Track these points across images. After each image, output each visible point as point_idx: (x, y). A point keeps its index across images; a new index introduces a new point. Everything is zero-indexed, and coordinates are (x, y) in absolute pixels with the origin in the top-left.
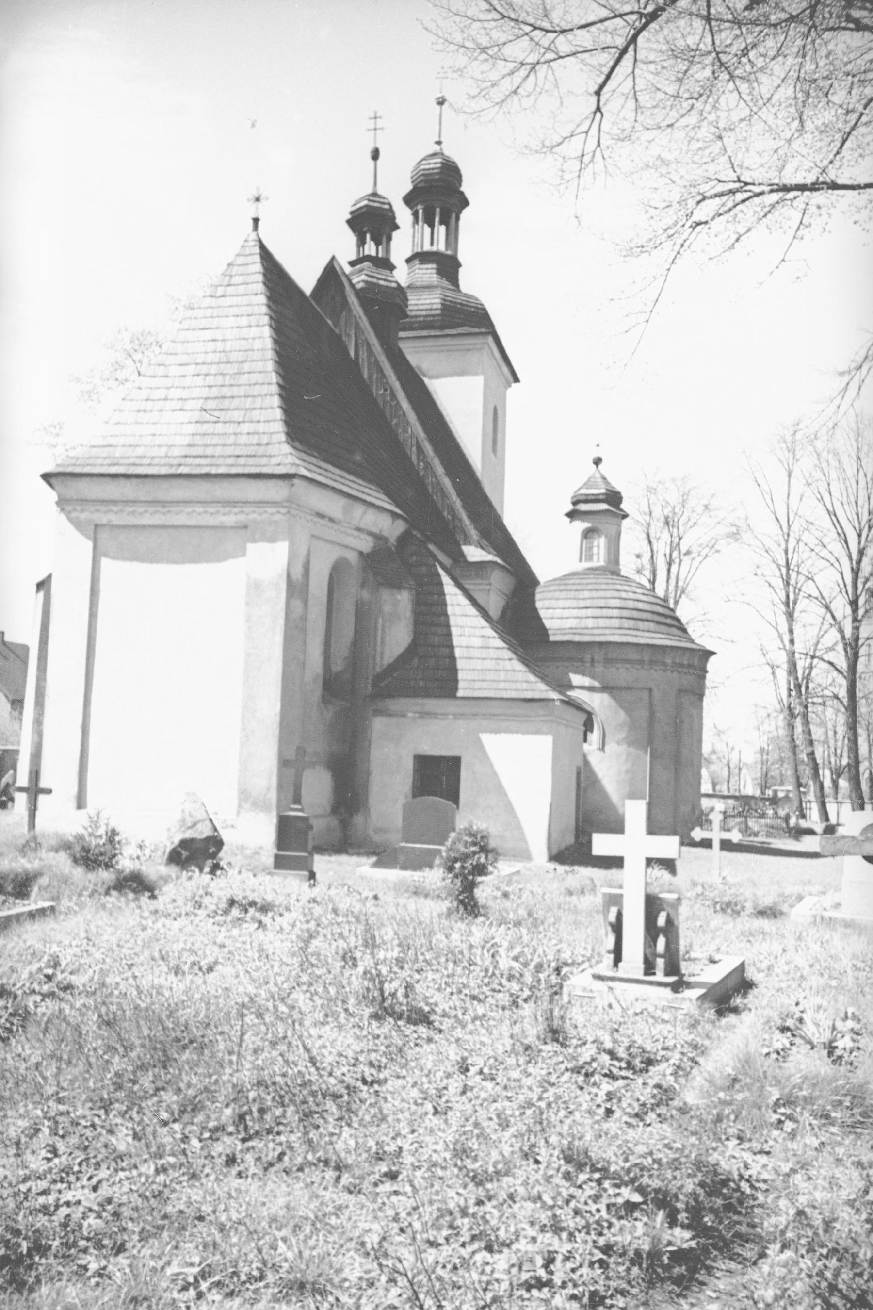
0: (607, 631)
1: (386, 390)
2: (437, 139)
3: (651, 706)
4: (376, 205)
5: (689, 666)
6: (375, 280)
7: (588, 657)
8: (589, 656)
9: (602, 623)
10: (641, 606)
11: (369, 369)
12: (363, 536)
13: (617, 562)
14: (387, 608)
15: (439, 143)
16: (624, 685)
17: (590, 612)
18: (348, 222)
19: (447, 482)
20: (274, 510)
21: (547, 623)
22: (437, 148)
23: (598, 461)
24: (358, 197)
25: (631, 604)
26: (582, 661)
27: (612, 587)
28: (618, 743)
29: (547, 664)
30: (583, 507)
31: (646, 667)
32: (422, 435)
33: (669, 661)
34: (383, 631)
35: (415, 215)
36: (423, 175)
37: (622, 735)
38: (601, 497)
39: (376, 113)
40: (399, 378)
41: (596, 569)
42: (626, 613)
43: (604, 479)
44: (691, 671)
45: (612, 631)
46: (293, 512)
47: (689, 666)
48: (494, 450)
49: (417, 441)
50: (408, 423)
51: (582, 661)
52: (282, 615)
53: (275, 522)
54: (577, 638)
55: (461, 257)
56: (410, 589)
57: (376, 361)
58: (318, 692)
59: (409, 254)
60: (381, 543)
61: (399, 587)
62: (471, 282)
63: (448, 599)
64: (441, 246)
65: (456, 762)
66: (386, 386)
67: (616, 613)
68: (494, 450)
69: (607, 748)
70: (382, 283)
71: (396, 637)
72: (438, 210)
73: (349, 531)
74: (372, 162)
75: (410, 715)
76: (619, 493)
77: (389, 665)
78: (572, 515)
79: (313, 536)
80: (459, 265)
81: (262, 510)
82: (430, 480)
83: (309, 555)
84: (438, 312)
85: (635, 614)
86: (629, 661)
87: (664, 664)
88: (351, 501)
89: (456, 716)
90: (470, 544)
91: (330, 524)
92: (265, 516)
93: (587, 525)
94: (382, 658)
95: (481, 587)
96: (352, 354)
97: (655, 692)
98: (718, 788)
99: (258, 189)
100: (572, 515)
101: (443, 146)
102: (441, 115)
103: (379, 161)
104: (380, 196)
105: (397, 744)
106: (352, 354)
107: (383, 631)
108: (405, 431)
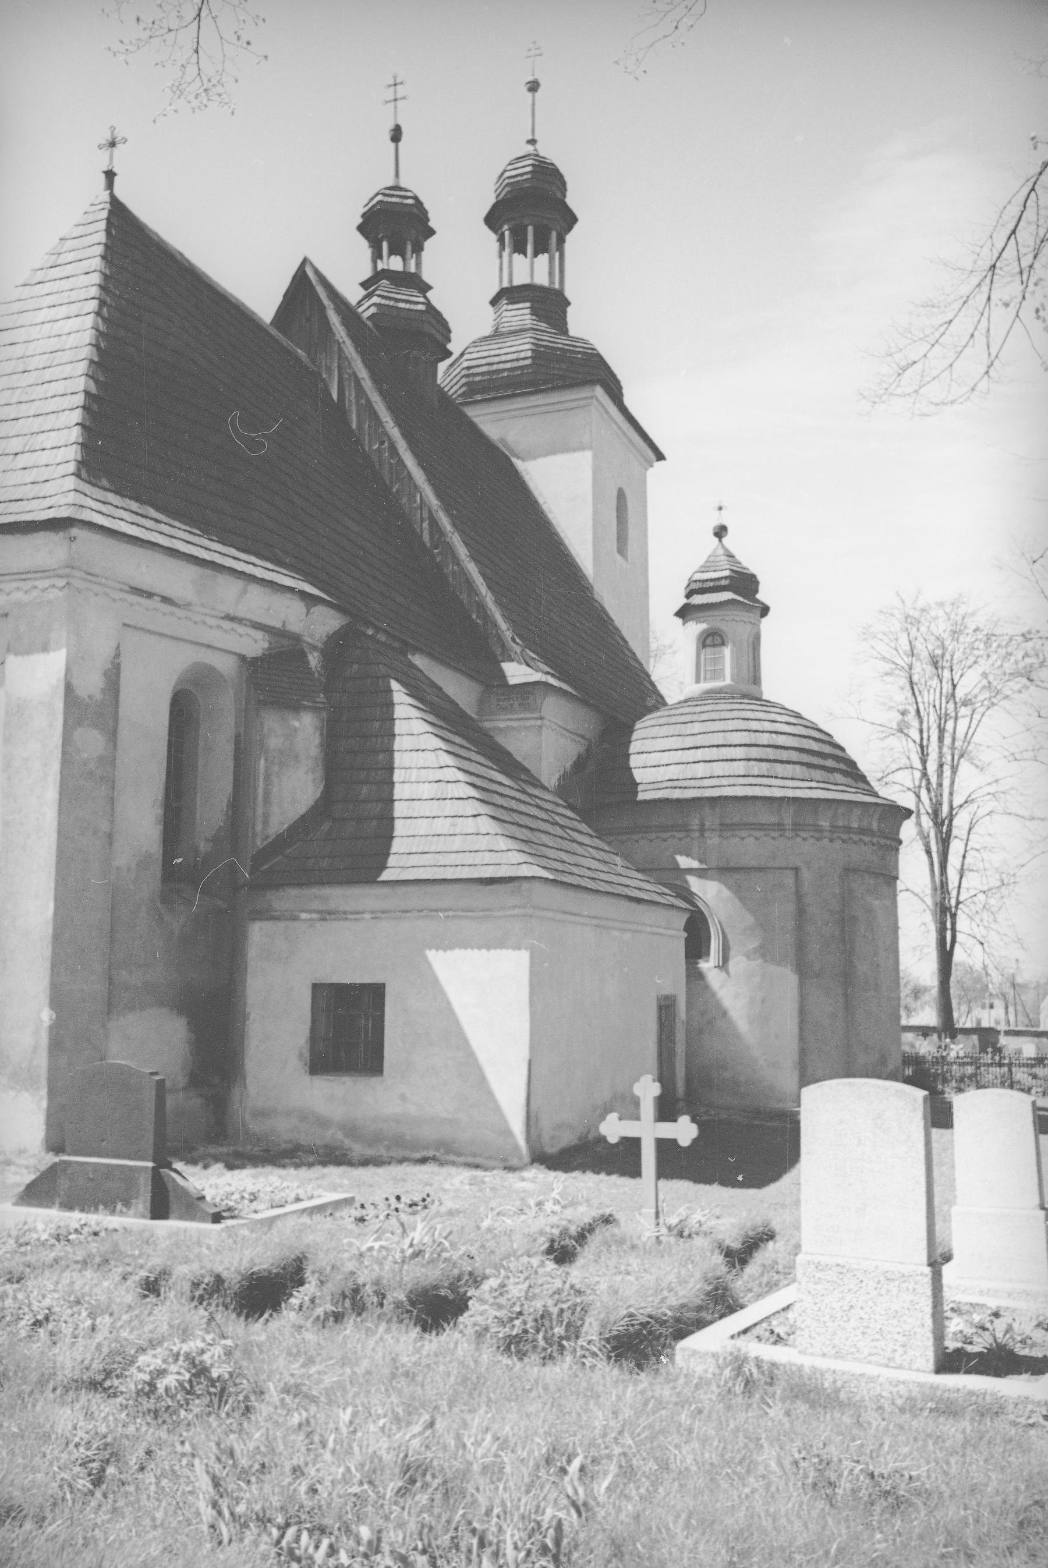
0: (724, 781)
1: (382, 443)
2: (530, 137)
3: (799, 897)
4: (394, 200)
5: (862, 831)
6: (392, 303)
7: (695, 823)
8: (697, 821)
9: (719, 769)
10: (781, 740)
11: (358, 415)
12: (241, 630)
13: (756, 680)
14: (274, 742)
15: (532, 142)
16: (754, 863)
17: (699, 754)
18: (361, 228)
19: (472, 568)
20: (46, 583)
21: (638, 775)
22: (530, 148)
23: (720, 532)
24: (372, 195)
25: (765, 739)
26: (686, 828)
27: (735, 714)
28: (748, 956)
29: (636, 837)
30: (698, 600)
32: (434, 501)
33: (825, 824)
34: (268, 777)
35: (501, 240)
36: (507, 184)
37: (754, 944)
38: (723, 583)
39: (395, 78)
40: (398, 423)
41: (720, 691)
42: (755, 752)
43: (731, 556)
44: (866, 839)
45: (732, 781)
46: (77, 583)
47: (862, 831)
48: (622, 550)
49: (430, 512)
50: (415, 486)
51: (686, 828)
52: (57, 754)
53: (49, 602)
54: (677, 794)
55: (568, 294)
56: (315, 710)
57: (368, 401)
58: (151, 882)
59: (495, 290)
60: (285, 642)
61: (296, 708)
62: (583, 323)
63: (399, 727)
64: (542, 279)
65: (377, 991)
66: (383, 436)
67: (739, 752)
68: (622, 550)
69: (731, 964)
70: (402, 305)
71: (293, 790)
72: (530, 229)
73: (211, 621)
74: (393, 145)
75: (303, 916)
76: (754, 576)
77: (279, 837)
78: (684, 613)
79: (125, 625)
80: (568, 303)
81: (30, 583)
82: (450, 568)
83: (118, 655)
84: (528, 362)
85: (771, 753)
87: (819, 829)
88: (208, 572)
89: (377, 915)
91: (166, 608)
92: (35, 593)
93: (703, 626)
94: (266, 823)
95: (528, 723)
96: (335, 396)
97: (806, 874)
99: (113, 128)
100: (684, 613)
101: (538, 146)
102: (533, 104)
103: (400, 144)
104: (401, 189)
105: (288, 964)
106: (335, 396)
107: (268, 777)
108: (411, 499)
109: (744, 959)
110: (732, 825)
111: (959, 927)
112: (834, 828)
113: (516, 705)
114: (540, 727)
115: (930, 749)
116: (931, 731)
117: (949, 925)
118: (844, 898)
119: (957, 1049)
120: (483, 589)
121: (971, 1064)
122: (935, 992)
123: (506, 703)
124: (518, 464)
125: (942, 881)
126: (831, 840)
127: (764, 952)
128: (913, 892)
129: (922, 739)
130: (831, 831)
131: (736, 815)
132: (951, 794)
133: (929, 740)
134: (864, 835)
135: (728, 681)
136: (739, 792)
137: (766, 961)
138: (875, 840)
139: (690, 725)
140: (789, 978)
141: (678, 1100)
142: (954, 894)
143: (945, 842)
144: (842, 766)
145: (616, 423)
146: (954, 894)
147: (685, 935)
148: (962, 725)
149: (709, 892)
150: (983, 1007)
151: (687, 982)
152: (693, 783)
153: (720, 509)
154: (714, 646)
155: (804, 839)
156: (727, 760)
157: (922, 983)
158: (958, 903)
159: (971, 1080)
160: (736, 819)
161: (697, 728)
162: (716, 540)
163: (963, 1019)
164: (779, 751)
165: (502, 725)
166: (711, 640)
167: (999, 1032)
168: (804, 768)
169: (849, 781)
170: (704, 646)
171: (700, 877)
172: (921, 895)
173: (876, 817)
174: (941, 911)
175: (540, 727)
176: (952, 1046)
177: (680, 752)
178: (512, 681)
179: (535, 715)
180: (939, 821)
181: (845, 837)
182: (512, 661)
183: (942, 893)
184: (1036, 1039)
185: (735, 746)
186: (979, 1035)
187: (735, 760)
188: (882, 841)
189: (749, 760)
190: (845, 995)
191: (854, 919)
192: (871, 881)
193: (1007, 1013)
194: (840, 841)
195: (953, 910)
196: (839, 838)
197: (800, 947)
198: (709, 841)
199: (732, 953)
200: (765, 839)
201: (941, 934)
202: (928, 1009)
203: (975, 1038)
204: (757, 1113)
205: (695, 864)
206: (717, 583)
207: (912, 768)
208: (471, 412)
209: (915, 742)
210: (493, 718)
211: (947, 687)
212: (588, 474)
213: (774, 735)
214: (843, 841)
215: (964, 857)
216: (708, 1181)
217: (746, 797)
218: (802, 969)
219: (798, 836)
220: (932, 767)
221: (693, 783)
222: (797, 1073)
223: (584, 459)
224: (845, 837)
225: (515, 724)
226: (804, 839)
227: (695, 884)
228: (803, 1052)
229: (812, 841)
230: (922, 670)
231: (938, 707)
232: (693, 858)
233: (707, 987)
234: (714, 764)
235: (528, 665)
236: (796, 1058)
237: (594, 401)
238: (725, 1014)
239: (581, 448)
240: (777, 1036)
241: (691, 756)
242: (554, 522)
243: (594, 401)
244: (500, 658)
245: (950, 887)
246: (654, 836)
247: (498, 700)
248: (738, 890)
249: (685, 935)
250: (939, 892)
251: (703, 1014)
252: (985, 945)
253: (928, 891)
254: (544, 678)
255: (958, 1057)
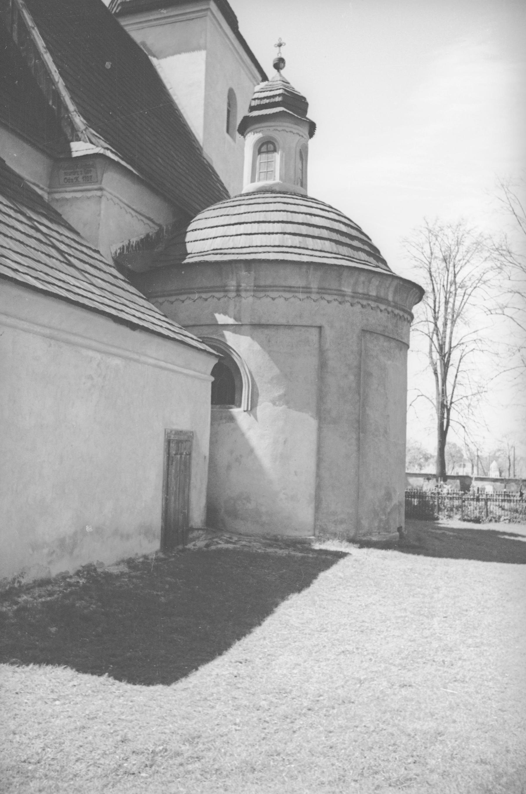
3: (322, 352)
5: (378, 299)
7: (232, 284)
8: (234, 283)
13: (303, 183)
16: (283, 321)
17: (242, 229)
19: (48, 58)
25: (300, 218)
26: (224, 289)
31: (314, 296)
33: (348, 290)
38: (278, 99)
42: (290, 228)
44: (383, 307)
47: (378, 299)
51: (224, 289)
54: (218, 258)
67: (277, 227)
85: (304, 230)
86: (290, 289)
87: (343, 295)
90: (78, 139)
95: (89, 194)
97: (328, 332)
98: (503, 474)
109: (271, 404)
110: (265, 286)
111: (452, 417)
112: (355, 294)
113: (80, 179)
114: (100, 197)
115: (440, 314)
116: (441, 304)
117: (445, 416)
118: (360, 355)
119: (447, 488)
120: (57, 76)
121: (458, 499)
122: (435, 458)
123: (72, 177)
124: (154, 61)
125: (443, 389)
126: (352, 305)
127: (287, 400)
128: (425, 396)
129: (435, 306)
130: (353, 297)
131: (268, 277)
132: (451, 338)
133: (439, 307)
134: (381, 303)
135: (277, 180)
136: (272, 257)
137: (289, 408)
138: (390, 309)
139: (238, 207)
140: (310, 423)
141: (192, 529)
142: (449, 398)
143: (446, 366)
144: (366, 248)
145: (229, 38)
146: (449, 398)
147: (212, 379)
148: (459, 299)
149: (243, 347)
150: (460, 466)
151: (212, 424)
152: (233, 251)
153: (280, 45)
154: (268, 152)
155: (329, 302)
156: (265, 233)
157: (429, 452)
158: (451, 403)
159: (458, 510)
160: (269, 282)
161: (243, 209)
162: (276, 71)
163: (449, 472)
164: (311, 228)
165: (68, 196)
166: (266, 146)
167: (471, 478)
168: (333, 244)
169: (371, 259)
170: (260, 152)
171: (235, 332)
172: (431, 399)
173: (392, 289)
174: (442, 407)
175: (100, 197)
176: (445, 486)
177: (226, 227)
178: (75, 155)
179: (95, 187)
180: (443, 354)
181: (365, 302)
182: (80, 140)
183: (443, 396)
184: (493, 483)
185: (274, 222)
186: (460, 480)
187: (273, 233)
188: (397, 311)
189: (284, 233)
190: (358, 439)
191: (369, 374)
192: (385, 344)
193: (473, 469)
194: (360, 306)
195: (448, 407)
196: (359, 303)
197: (321, 397)
198: (243, 300)
199: (260, 399)
200: (292, 300)
201: (441, 421)
202: (431, 465)
203: (458, 481)
204: (275, 541)
205: (231, 321)
206: (272, 100)
207: (427, 321)
208: (123, 22)
209: (430, 307)
210: (61, 189)
211: (451, 276)
212: (203, 67)
213: (308, 216)
214: (363, 306)
215: (456, 376)
216: (96, 670)
217: (277, 260)
218: (321, 415)
219: (323, 298)
220: (440, 324)
221: (233, 251)
222: (313, 505)
223: (201, 56)
224: (365, 302)
225: (78, 195)
226: (329, 302)
227: (231, 339)
228: (319, 487)
229: (336, 303)
230: (438, 265)
231: (445, 287)
232: (231, 317)
233: (237, 428)
234: (253, 236)
235: (91, 143)
236: (313, 492)
237: (209, 13)
238: (252, 451)
239: (198, 48)
240: (296, 473)
241: (233, 230)
242: (177, 102)
243: (209, 13)
244: (70, 138)
245: (448, 395)
246: (197, 296)
247: (66, 174)
248: (267, 346)
249: (212, 379)
250: (441, 396)
251: (231, 452)
252: (466, 428)
253: (435, 395)
254: (101, 151)
255: (448, 494)
